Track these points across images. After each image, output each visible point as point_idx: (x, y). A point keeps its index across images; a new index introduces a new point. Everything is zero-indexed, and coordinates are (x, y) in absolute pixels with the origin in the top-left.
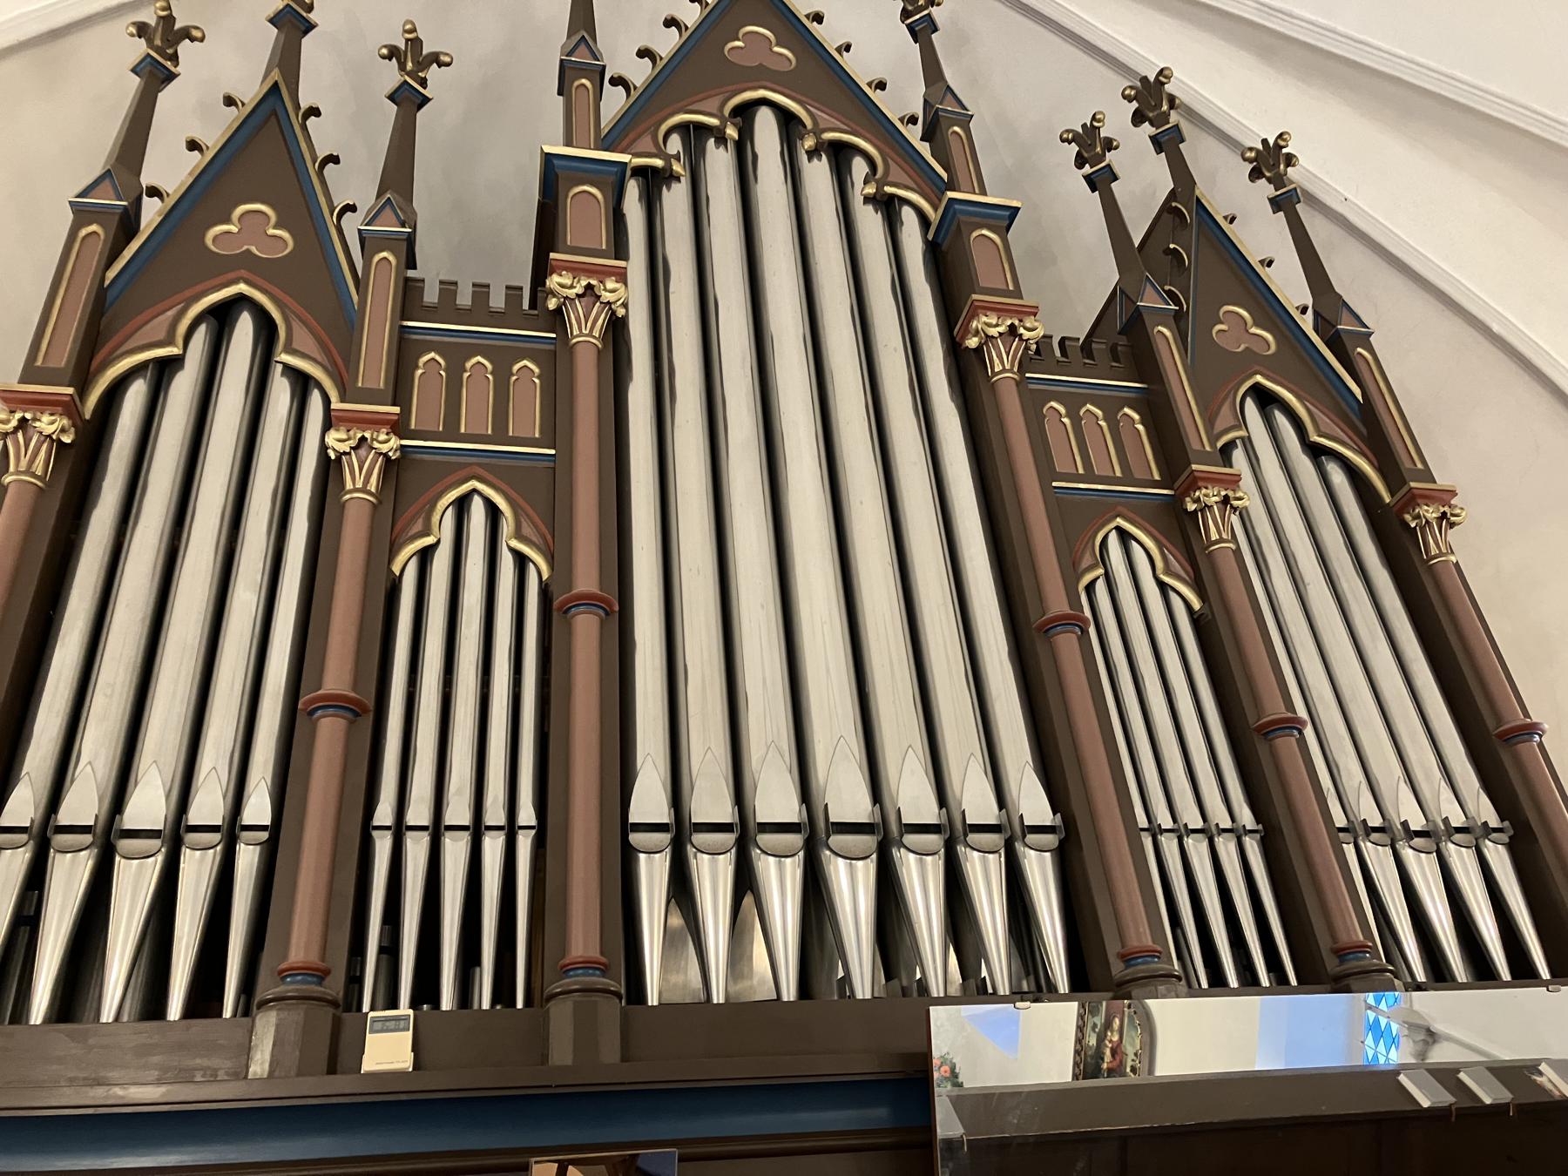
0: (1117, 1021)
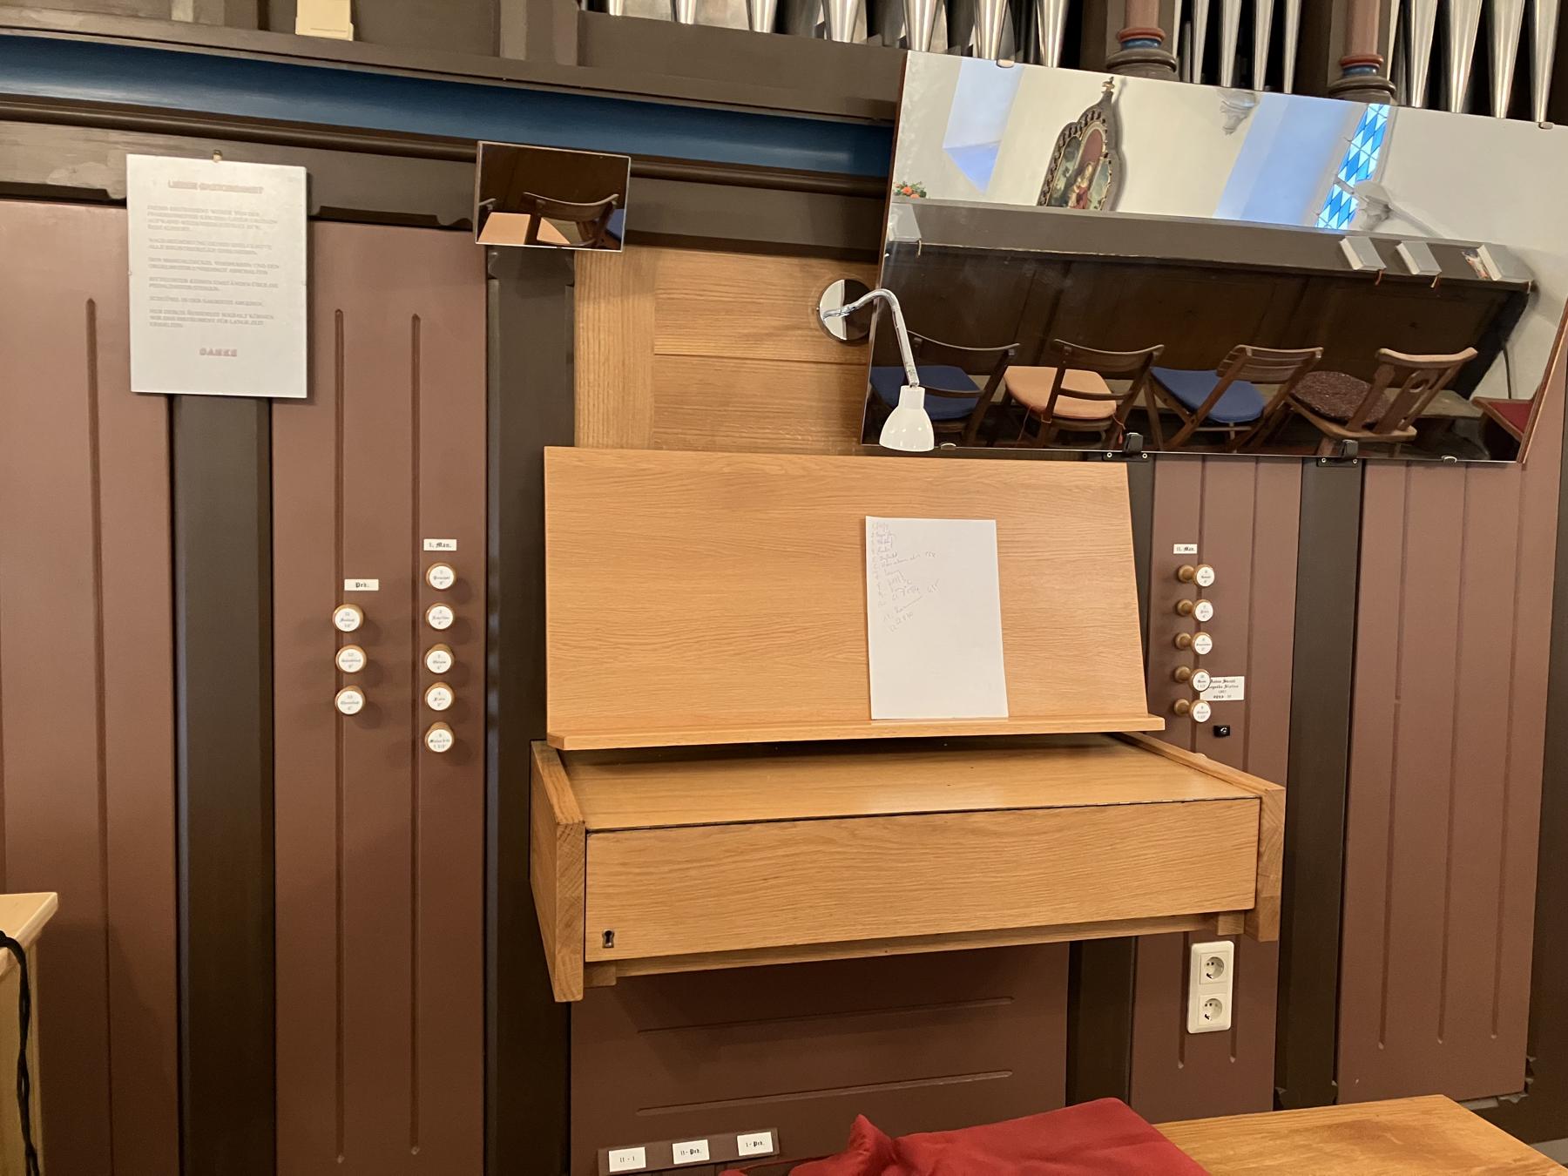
0: (1090, 169)
